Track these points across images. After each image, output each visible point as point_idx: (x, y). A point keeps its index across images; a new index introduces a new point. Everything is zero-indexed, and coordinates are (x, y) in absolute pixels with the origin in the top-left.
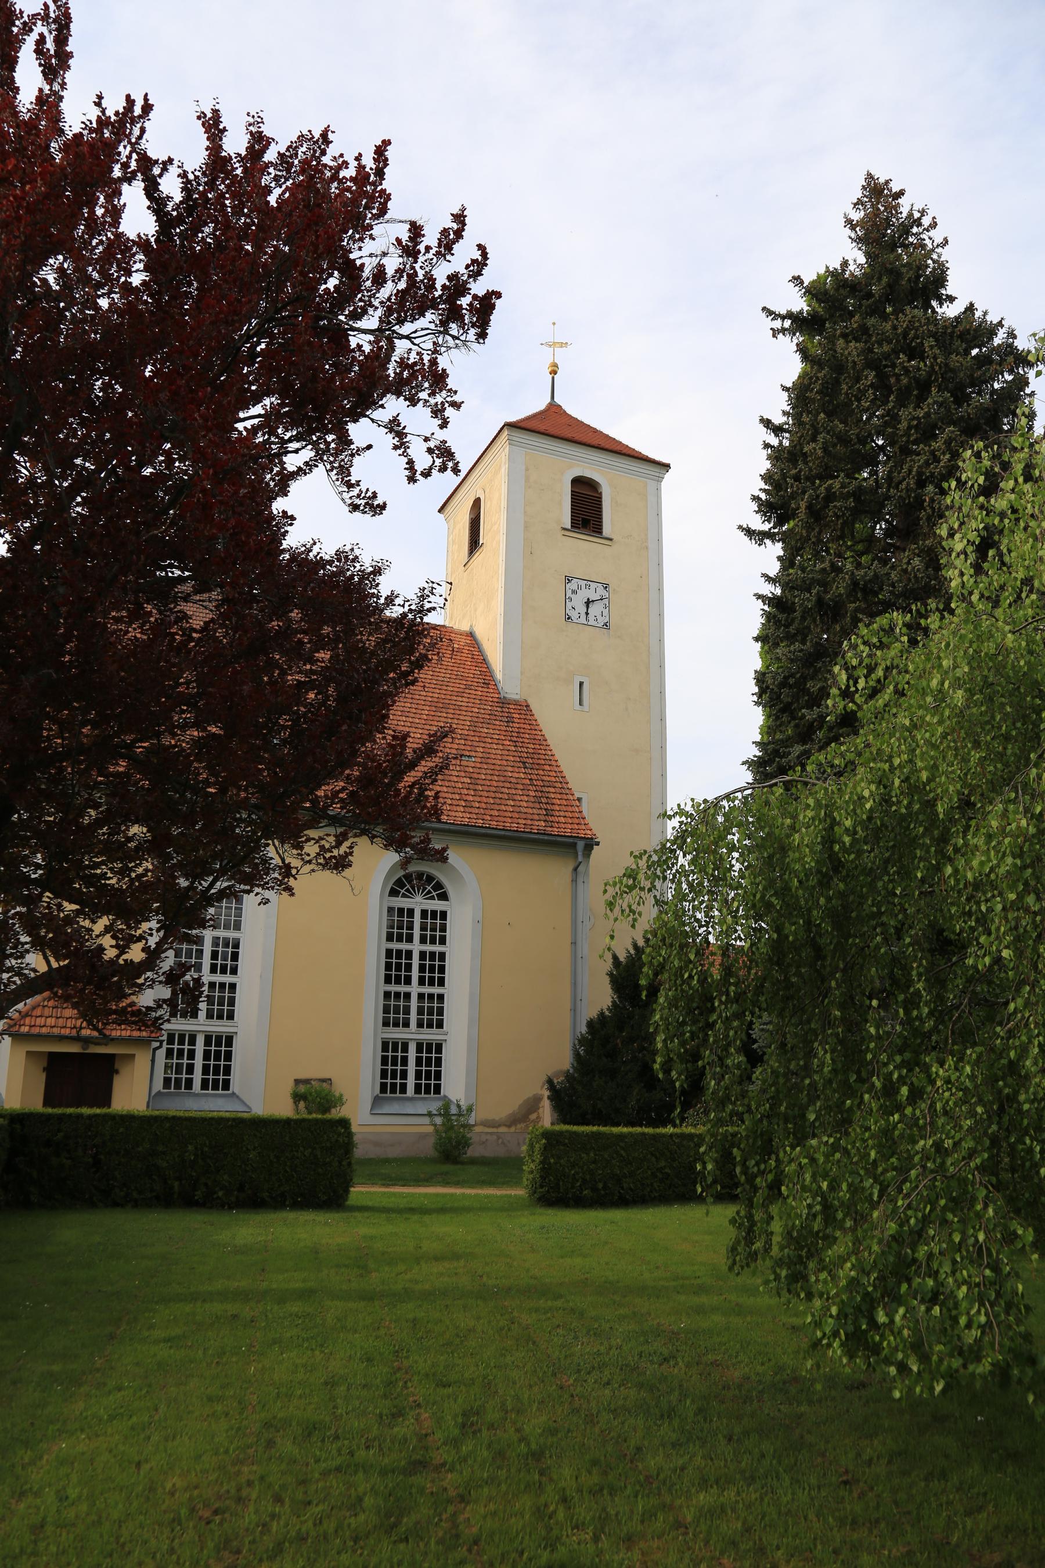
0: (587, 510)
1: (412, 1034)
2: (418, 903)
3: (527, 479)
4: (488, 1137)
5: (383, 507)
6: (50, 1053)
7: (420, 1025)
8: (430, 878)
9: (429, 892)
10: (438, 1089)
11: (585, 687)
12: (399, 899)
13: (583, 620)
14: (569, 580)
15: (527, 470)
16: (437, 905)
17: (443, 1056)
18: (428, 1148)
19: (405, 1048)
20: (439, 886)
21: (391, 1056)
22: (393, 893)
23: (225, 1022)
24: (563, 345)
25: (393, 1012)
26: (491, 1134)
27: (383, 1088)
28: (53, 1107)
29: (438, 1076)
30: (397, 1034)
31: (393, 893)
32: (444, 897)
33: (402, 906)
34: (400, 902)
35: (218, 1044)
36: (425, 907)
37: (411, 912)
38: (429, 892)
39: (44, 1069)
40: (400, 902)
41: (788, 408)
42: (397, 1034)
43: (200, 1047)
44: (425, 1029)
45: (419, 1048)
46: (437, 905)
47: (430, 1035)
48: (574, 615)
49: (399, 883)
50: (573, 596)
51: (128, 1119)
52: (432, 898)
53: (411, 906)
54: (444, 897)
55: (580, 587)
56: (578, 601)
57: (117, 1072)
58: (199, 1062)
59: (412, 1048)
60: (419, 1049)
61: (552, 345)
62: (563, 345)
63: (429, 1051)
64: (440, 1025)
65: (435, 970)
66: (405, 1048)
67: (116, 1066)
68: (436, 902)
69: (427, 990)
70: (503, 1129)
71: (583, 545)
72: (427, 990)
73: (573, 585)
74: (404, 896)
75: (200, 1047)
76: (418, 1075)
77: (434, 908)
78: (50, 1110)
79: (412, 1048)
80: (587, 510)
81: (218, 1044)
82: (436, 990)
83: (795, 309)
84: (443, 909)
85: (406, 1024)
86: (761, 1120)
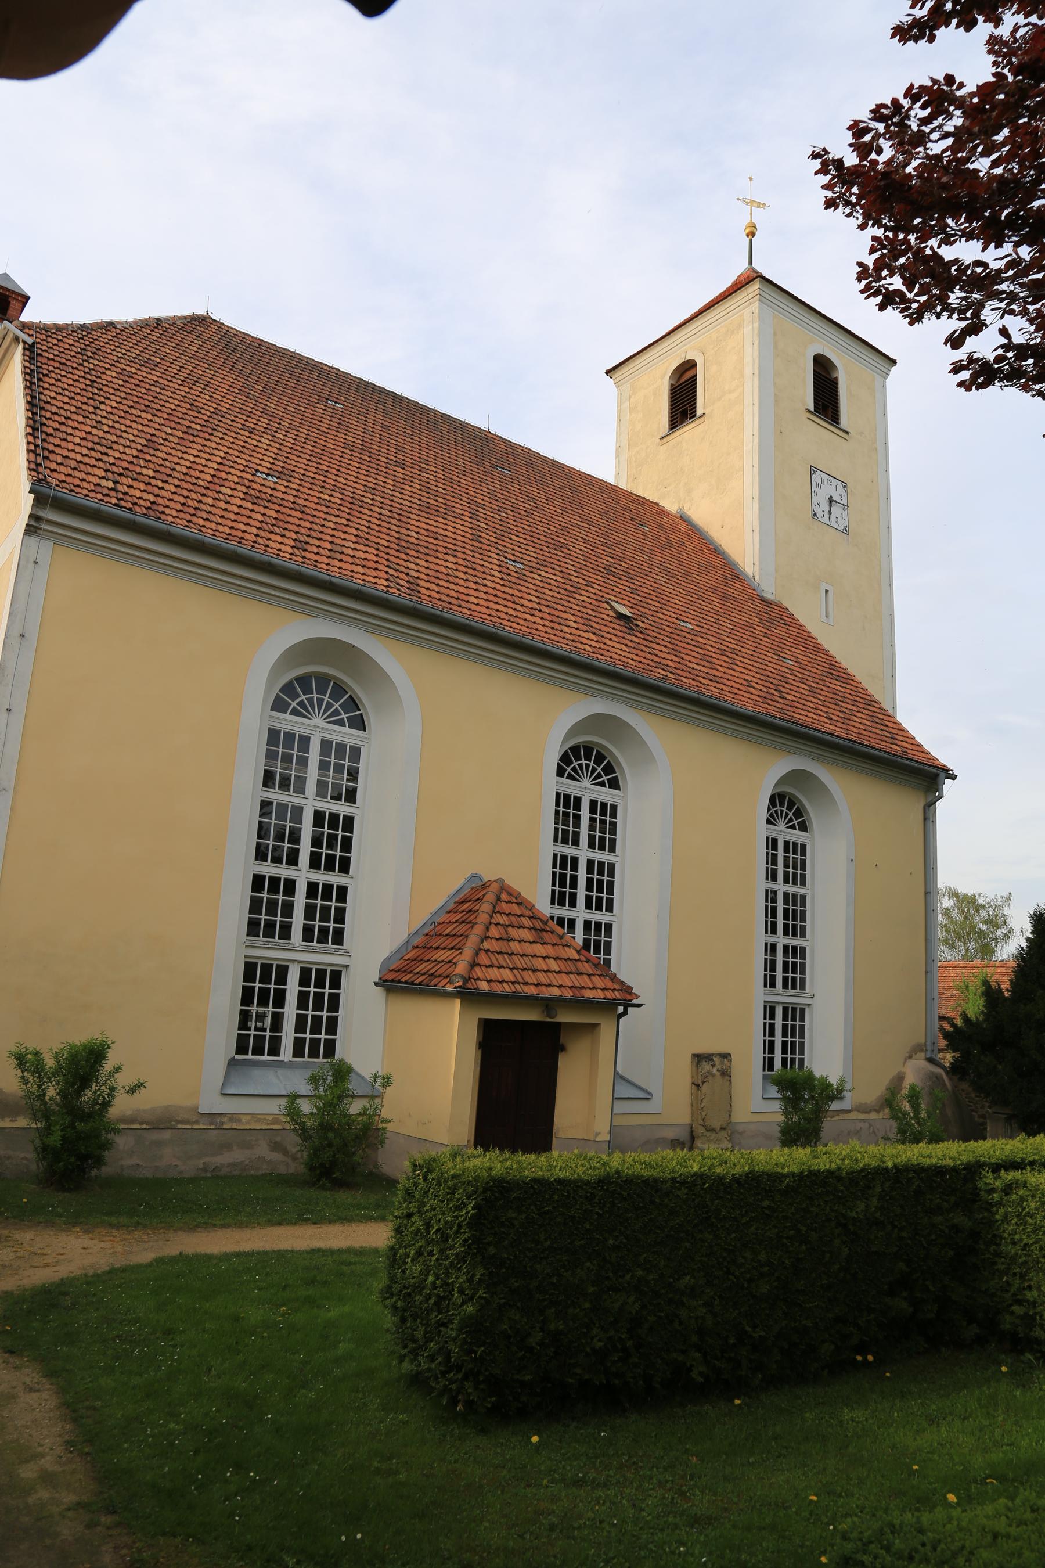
0: (826, 401)
1: (296, 953)
2: (317, 728)
3: (776, 347)
4: (862, 1125)
8: (339, 690)
9: (336, 713)
10: (330, 1048)
11: (830, 593)
13: (826, 520)
15: (775, 334)
17: (241, 984)
18: (292, 1160)
19: (282, 975)
20: (353, 704)
21: (260, 984)
22: (279, 705)
24: (761, 205)
25: (266, 909)
26: (864, 1120)
27: (241, 1048)
29: (332, 1026)
31: (279, 705)
34: (287, 722)
35: (265, 978)
37: (305, 741)
38: (336, 713)
40: (287, 722)
42: (270, 952)
43: (292, 987)
46: (347, 735)
48: (819, 514)
49: (288, 689)
50: (817, 490)
52: (340, 723)
54: (359, 723)
56: (822, 497)
57: (563, 1049)
58: (290, 1010)
60: (304, 980)
61: (751, 203)
62: (761, 205)
63: (320, 984)
64: (339, 937)
65: (335, 843)
66: (282, 978)
67: (562, 1041)
68: (347, 729)
69: (322, 877)
70: (873, 1115)
71: (818, 431)
73: (818, 477)
74: (295, 712)
75: (292, 987)
76: (300, 1024)
80: (826, 401)
81: (265, 978)
82: (335, 879)
83: (835, 153)
85: (286, 931)
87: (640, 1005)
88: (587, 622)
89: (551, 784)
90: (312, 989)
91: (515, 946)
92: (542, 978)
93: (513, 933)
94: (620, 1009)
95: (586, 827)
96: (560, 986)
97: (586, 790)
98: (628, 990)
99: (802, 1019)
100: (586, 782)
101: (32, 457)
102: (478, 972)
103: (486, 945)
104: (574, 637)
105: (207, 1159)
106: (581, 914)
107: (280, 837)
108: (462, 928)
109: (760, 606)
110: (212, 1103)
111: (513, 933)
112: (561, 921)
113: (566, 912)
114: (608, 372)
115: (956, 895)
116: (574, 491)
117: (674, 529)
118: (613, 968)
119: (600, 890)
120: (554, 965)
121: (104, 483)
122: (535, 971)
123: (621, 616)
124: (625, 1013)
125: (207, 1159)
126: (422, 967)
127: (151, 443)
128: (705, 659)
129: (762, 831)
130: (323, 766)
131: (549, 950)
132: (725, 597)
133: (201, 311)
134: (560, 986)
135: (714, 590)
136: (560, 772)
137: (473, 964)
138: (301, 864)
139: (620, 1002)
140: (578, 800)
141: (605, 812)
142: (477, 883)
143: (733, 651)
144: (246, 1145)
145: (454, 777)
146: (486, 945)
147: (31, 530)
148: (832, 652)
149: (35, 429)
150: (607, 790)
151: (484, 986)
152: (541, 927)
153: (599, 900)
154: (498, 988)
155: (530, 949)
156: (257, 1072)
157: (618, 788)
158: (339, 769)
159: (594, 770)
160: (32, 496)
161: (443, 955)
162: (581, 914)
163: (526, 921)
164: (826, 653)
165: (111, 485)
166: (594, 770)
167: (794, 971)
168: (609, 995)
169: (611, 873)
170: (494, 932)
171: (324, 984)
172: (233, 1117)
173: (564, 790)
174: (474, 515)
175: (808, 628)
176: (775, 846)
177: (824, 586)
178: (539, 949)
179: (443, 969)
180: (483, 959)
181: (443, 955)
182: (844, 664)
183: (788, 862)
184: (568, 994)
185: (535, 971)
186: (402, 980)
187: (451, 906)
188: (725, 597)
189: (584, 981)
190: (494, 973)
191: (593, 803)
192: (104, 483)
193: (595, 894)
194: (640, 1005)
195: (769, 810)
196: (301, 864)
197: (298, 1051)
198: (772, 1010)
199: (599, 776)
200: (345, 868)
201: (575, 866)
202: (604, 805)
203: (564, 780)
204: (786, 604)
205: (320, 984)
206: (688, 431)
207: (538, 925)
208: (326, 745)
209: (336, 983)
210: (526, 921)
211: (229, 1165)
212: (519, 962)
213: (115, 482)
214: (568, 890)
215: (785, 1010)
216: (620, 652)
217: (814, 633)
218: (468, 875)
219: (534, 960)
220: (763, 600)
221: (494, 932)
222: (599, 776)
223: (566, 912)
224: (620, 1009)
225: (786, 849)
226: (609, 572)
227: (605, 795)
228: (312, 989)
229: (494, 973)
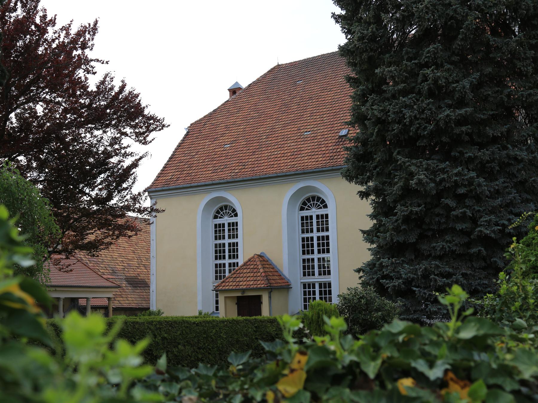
1: (317, 279)
2: (314, 212)
5: (96, 73)
6: (237, 297)
7: (320, 274)
16: (233, 220)
23: (311, 277)
28: (242, 316)
30: (309, 280)
33: (307, 215)
36: (318, 213)
39: (236, 304)
42: (309, 280)
43: (317, 289)
44: (322, 276)
45: (320, 286)
46: (233, 220)
47: (324, 279)
52: (321, 208)
53: (311, 214)
59: (317, 286)
60: (320, 286)
63: (325, 287)
74: (307, 209)
75: (317, 289)
78: (240, 318)
79: (317, 286)
84: (326, 213)
86: (212, 338)
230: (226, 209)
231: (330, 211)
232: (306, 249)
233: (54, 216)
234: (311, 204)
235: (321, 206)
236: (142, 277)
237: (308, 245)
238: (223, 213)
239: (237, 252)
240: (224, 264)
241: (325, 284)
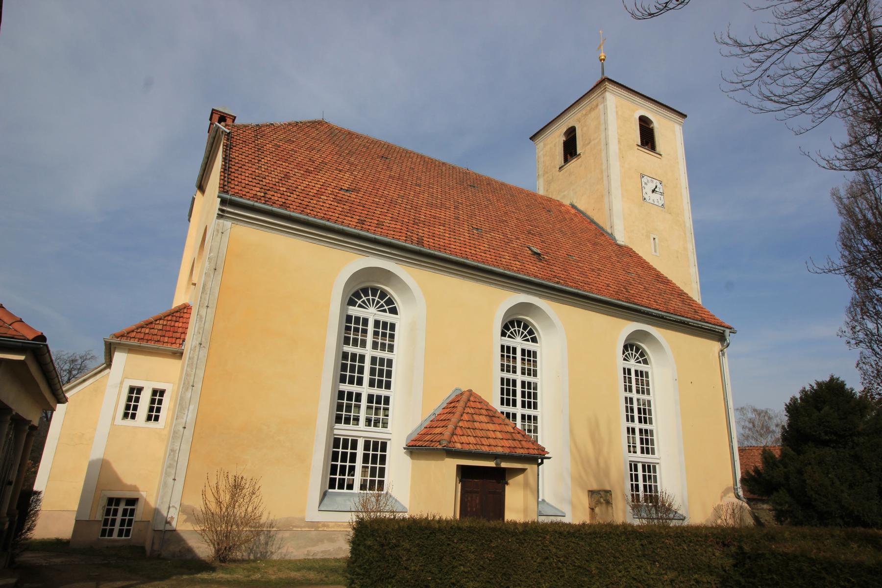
1: (360, 432)
2: (372, 313)
9: (382, 306)
12: (356, 308)
14: (642, 176)
16: (388, 317)
20: (390, 302)
23: (380, 429)
25: (343, 408)
30: (343, 430)
32: (394, 311)
34: (354, 311)
35: (345, 446)
36: (378, 318)
37: (365, 321)
41: (843, 193)
42: (343, 430)
43: (360, 452)
44: (372, 428)
46: (388, 317)
47: (376, 434)
49: (357, 295)
51: (56, 546)
52: (385, 311)
53: (366, 316)
55: (648, 181)
59: (640, 466)
63: (375, 449)
65: (383, 374)
69: (376, 391)
72: (376, 391)
73: (645, 179)
74: (360, 306)
75: (360, 452)
77: (386, 320)
82: (383, 392)
84: (393, 321)
87: (549, 458)
88: (515, 257)
89: (498, 341)
90: (371, 452)
91: (477, 425)
92: (492, 442)
93: (476, 417)
94: (540, 461)
95: (519, 362)
96: (503, 447)
97: (518, 343)
98: (543, 449)
99: (655, 472)
100: (519, 339)
101: (222, 182)
102: (455, 438)
103: (460, 424)
104: (507, 264)
105: (309, 549)
106: (519, 410)
107: (353, 369)
108: (449, 416)
109: (616, 248)
110: (313, 515)
111: (476, 417)
112: (508, 414)
113: (510, 409)
114: (531, 138)
115: (755, 410)
116: (512, 196)
117: (568, 212)
118: (539, 443)
119: (529, 397)
120: (499, 435)
121: (259, 194)
122: (488, 438)
123: (535, 253)
124: (542, 463)
125: (309, 549)
126: (428, 437)
127: (287, 176)
128: (582, 273)
129: (620, 364)
130: (376, 334)
131: (498, 427)
132: (595, 244)
133: (318, 118)
134: (503, 447)
135: (589, 241)
136: (503, 334)
137: (453, 434)
138: (360, 380)
139: (537, 457)
140: (514, 349)
141: (528, 355)
142: (458, 393)
143: (599, 270)
144: (332, 540)
145: (444, 334)
146: (460, 424)
147: (220, 216)
148: (658, 269)
149: (225, 170)
150: (530, 343)
151: (458, 446)
152: (492, 415)
153: (529, 403)
154: (467, 448)
155: (485, 426)
156: (339, 499)
157: (537, 342)
158: (384, 335)
159: (523, 333)
160: (219, 200)
161: (438, 430)
162: (519, 410)
163: (484, 412)
164: (654, 269)
165: (262, 194)
166: (523, 333)
167: (647, 444)
168: (531, 451)
169: (535, 388)
170: (465, 417)
171: (377, 452)
172: (325, 525)
173: (506, 344)
174: (456, 208)
175: (644, 258)
176: (629, 373)
177: (652, 236)
178: (491, 427)
179: (438, 438)
180: (459, 431)
181: (438, 430)
182: (666, 275)
183: (638, 381)
184: (507, 451)
185: (488, 438)
186: (417, 448)
187: (445, 405)
188: (595, 244)
189: (516, 444)
190: (464, 439)
191: (523, 351)
192: (259, 194)
193: (526, 399)
194: (549, 458)
195: (624, 353)
196: (360, 380)
197: (363, 487)
198: (636, 466)
199: (526, 336)
200: (388, 386)
201: (514, 385)
202: (529, 352)
203: (506, 338)
204: (631, 247)
205: (375, 449)
206: (574, 163)
207: (491, 414)
208: (377, 323)
209: (384, 449)
210: (484, 412)
211: (322, 552)
212: (479, 433)
213: (265, 193)
214: (511, 397)
215: (644, 466)
216: (534, 271)
217: (647, 260)
218: (454, 389)
219: (488, 433)
220: (617, 245)
221: (465, 417)
222: (526, 336)
223: (510, 409)
224: (540, 461)
225: (637, 375)
226: (530, 233)
227: (530, 346)
228: (371, 452)
229: (464, 439)
230: (374, 295)
231: (402, 321)
232: (384, 379)
233: (725, 340)
234: (373, 300)
235: (386, 308)
236: (760, 452)
237: (381, 371)
238: (378, 302)
239: (502, 389)
240: (359, 396)
241: (376, 443)
